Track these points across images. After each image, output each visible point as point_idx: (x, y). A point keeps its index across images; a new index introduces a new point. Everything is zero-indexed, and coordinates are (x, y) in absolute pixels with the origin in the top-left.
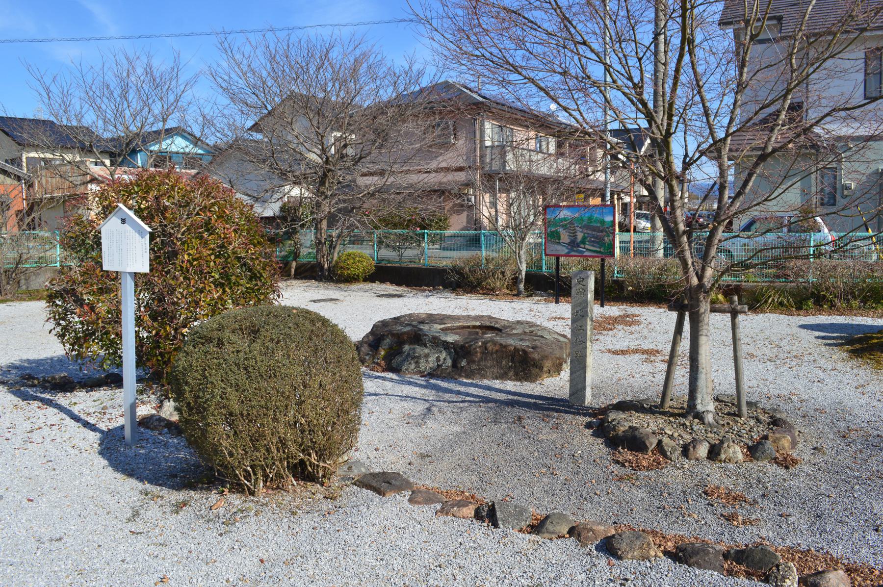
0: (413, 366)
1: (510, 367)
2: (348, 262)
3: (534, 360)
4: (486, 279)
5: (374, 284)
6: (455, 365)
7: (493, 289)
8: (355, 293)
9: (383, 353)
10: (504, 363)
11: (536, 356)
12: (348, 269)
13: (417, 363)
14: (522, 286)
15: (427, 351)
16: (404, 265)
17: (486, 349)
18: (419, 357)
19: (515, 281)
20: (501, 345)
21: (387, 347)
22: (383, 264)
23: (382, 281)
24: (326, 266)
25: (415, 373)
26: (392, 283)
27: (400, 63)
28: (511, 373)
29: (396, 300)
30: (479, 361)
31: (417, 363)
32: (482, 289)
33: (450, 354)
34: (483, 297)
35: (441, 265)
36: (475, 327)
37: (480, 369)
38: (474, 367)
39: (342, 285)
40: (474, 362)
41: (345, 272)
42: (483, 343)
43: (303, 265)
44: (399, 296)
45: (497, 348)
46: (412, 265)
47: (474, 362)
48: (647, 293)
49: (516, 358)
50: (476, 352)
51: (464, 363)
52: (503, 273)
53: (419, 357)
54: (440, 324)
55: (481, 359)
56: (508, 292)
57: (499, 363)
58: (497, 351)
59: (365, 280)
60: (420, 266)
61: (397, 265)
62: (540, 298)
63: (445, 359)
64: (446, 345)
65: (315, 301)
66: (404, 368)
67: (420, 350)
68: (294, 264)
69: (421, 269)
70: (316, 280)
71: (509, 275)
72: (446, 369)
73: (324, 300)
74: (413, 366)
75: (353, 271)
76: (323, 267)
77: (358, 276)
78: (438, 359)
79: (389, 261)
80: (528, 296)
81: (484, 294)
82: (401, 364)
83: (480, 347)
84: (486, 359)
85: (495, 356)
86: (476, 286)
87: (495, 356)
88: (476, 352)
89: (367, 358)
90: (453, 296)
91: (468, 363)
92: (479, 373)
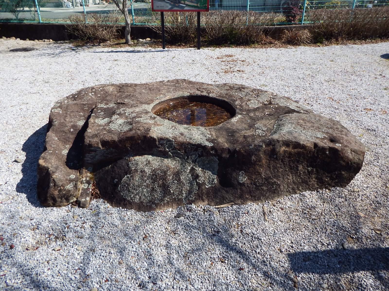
28: (313, 181)
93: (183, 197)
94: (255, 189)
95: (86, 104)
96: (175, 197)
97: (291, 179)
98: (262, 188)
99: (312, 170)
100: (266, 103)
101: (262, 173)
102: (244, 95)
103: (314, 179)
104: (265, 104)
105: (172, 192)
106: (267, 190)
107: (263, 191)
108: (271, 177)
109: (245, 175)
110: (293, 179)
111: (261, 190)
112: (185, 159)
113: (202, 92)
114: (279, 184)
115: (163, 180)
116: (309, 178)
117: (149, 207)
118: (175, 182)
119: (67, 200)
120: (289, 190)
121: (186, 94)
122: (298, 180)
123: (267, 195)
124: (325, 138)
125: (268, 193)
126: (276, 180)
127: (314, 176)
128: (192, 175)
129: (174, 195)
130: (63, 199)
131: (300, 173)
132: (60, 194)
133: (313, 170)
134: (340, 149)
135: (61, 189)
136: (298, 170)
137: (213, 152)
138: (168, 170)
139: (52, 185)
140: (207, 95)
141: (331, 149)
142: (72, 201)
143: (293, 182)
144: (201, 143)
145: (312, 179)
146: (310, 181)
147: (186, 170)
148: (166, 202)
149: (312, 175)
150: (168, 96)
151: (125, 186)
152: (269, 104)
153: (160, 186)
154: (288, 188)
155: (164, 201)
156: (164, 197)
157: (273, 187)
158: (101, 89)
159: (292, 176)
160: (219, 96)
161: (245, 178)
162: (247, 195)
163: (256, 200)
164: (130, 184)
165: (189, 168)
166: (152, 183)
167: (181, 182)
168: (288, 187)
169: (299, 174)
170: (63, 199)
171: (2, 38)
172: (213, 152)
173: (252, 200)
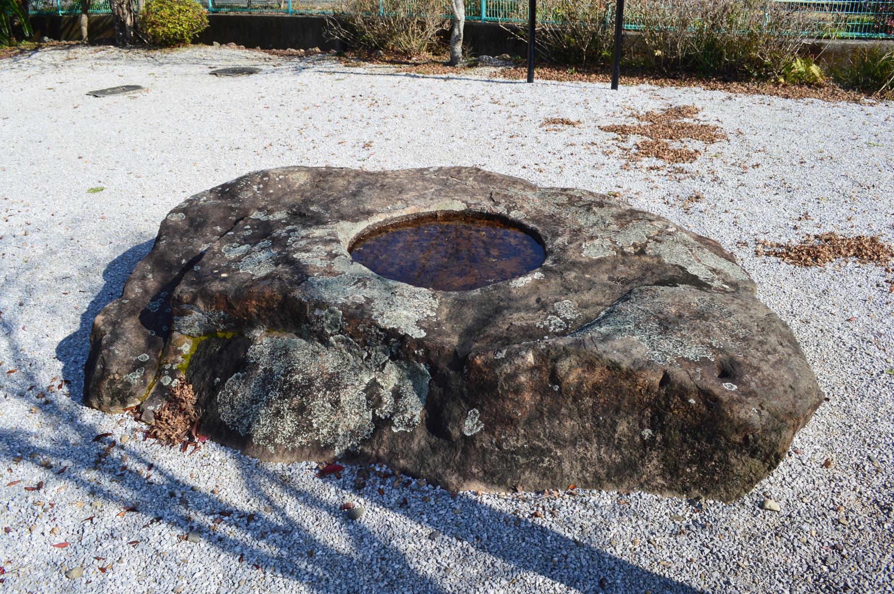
0: (288, 425)
1: (647, 445)
2: (162, 13)
3: (745, 426)
4: (392, 34)
5: (209, 48)
6: (437, 421)
7: (406, 53)
8: (176, 68)
9: (187, 348)
10: (622, 427)
11: (750, 413)
12: (164, 25)
13: (301, 410)
14: (458, 48)
15: (329, 361)
16: (255, 13)
17: (554, 377)
18: (306, 388)
19: (445, 37)
20: (614, 367)
21: (196, 330)
22: (223, 12)
23: (224, 42)
24: (129, 22)
25: (301, 453)
26: (238, 43)
27: (341, 300)
28: (652, 465)
29: (243, 79)
30: (529, 423)
31: (301, 410)
32: (387, 52)
33: (414, 375)
34: (392, 69)
35: (314, 12)
36: (449, 216)
37: (534, 450)
38: (514, 441)
39: (158, 53)
40: (511, 422)
41: (160, 30)
42: (542, 357)
43: (101, 19)
44: (250, 72)
45: (597, 376)
46: (268, 13)
47: (511, 422)
48: (687, 59)
49: (675, 415)
50: (518, 390)
51: (471, 425)
52: (422, 24)
53: (306, 388)
54: (354, 218)
55: (538, 415)
56: (429, 56)
57: (604, 434)
58: (596, 388)
59: (195, 41)
60: (281, 14)
61: (245, 14)
62: (493, 69)
63: (397, 394)
64: (397, 345)
65: (96, 94)
66: (260, 431)
67: (314, 360)
68: (84, 19)
69: (282, 18)
70: (116, 45)
71: (432, 29)
72: (408, 437)
73: (113, 91)
74: (288, 425)
75: (172, 28)
76: (123, 23)
77: (182, 35)
78: (372, 389)
79: (231, 7)
80: (470, 66)
81: (392, 62)
82: (248, 413)
83: (532, 369)
84: (554, 413)
85: (588, 401)
86: (377, 48)
87: (588, 401)
88: (518, 390)
89: (135, 378)
90: (340, 67)
91: (489, 429)
92: (533, 467)
93: (336, 441)
94: (498, 456)
95: (236, 208)
96: (319, 440)
97: (594, 450)
98: (512, 458)
99: (653, 439)
100: (631, 250)
101: (518, 422)
102: (590, 223)
103: (655, 462)
104: (624, 254)
105: (315, 425)
106: (527, 464)
107: (516, 465)
108: (542, 436)
109: (479, 419)
110: (599, 450)
111: (510, 462)
112: (362, 358)
113: (497, 204)
114: (559, 458)
115: (302, 397)
116: (642, 457)
117: (261, 449)
118: (326, 405)
119: (124, 403)
120: (584, 477)
121: (458, 206)
122: (614, 456)
123: (523, 477)
124: (704, 362)
125: (527, 473)
126: (552, 446)
127: (655, 454)
128: (368, 398)
129: (318, 435)
130: (116, 398)
131: (620, 440)
132: (111, 388)
133: (655, 438)
134: (725, 398)
135: (115, 379)
136: (615, 431)
137: (421, 354)
138: (318, 377)
139: (99, 367)
140: (505, 212)
141: (706, 395)
142: (133, 405)
143: (600, 460)
144: (399, 328)
145: (650, 461)
146: (643, 466)
147: (357, 384)
148: (297, 445)
149: (650, 450)
150: (413, 207)
151: (228, 394)
152: (636, 254)
153: (293, 409)
154: (581, 472)
155: (294, 441)
156: (296, 434)
157: (543, 461)
158: (281, 177)
159: (599, 443)
160: (533, 219)
161: (478, 426)
162: (476, 468)
163: (493, 483)
164: (237, 393)
165: (367, 380)
166: (280, 398)
167: (340, 408)
168: (584, 468)
169: (616, 441)
170: (116, 398)
171: (212, 44)
172: (421, 354)
173: (485, 481)
